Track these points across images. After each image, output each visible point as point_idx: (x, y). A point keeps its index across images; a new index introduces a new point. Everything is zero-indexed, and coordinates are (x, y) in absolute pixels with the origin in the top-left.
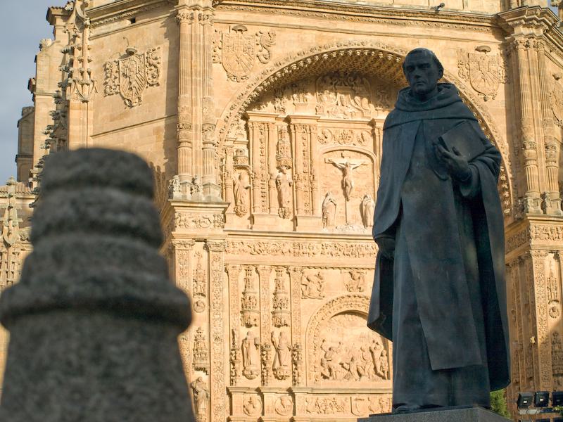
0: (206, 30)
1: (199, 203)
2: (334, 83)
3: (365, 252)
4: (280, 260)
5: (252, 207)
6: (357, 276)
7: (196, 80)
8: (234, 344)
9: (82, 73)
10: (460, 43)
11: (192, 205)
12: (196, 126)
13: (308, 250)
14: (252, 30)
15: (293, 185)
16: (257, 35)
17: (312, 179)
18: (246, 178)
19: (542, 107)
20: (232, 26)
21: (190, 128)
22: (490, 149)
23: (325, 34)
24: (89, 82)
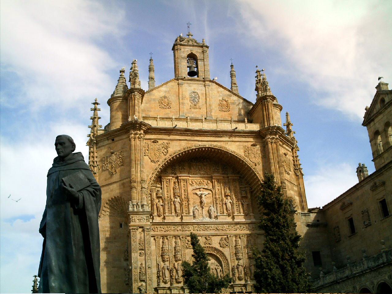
0: (141, 143)
1: (139, 212)
2: (195, 162)
3: (211, 229)
4: (176, 233)
5: (164, 213)
6: (208, 239)
7: (137, 163)
8: (159, 269)
9: (94, 162)
10: (244, 143)
11: (137, 213)
12: (138, 181)
13: (188, 229)
14: (160, 142)
15: (181, 205)
16: (162, 144)
17: (188, 201)
18: (161, 201)
19: (279, 167)
20: (152, 141)
21: (135, 182)
22: (94, 184)
23: (190, 142)
24: (97, 166)
